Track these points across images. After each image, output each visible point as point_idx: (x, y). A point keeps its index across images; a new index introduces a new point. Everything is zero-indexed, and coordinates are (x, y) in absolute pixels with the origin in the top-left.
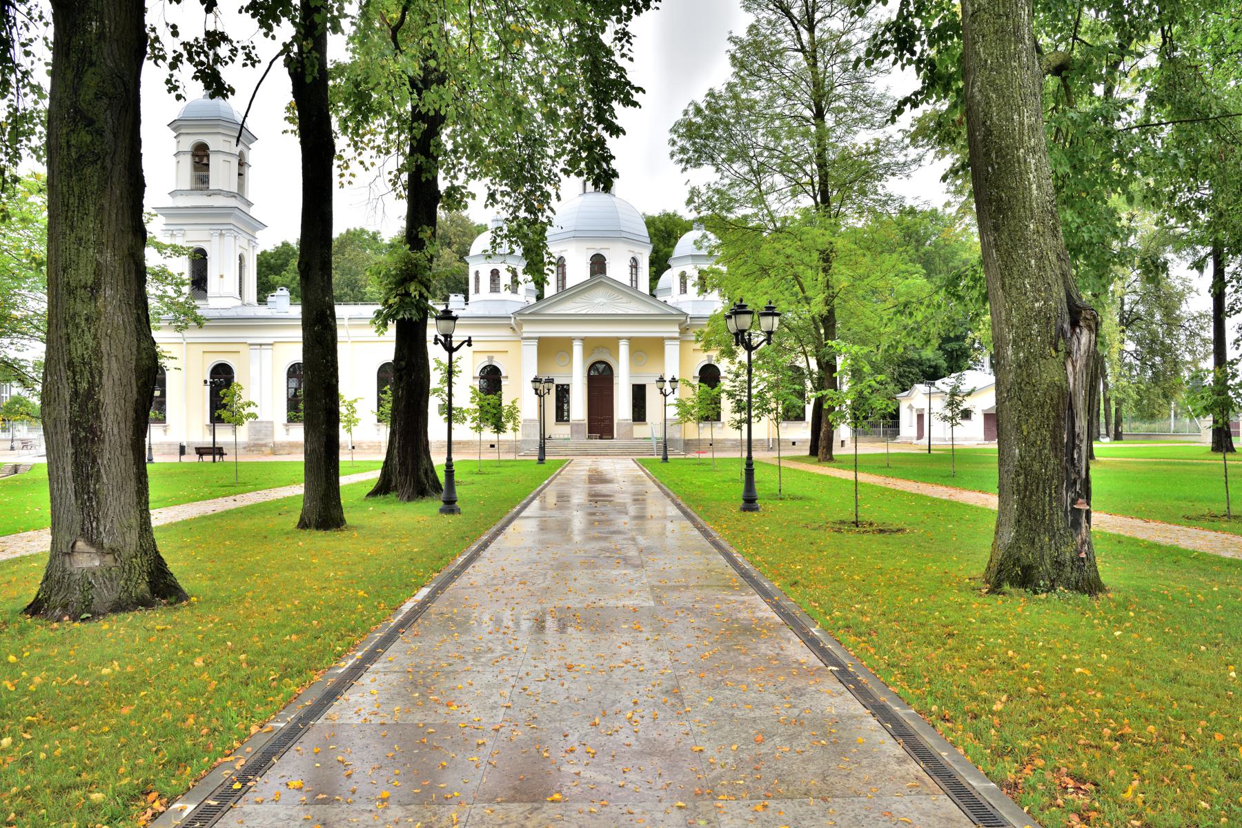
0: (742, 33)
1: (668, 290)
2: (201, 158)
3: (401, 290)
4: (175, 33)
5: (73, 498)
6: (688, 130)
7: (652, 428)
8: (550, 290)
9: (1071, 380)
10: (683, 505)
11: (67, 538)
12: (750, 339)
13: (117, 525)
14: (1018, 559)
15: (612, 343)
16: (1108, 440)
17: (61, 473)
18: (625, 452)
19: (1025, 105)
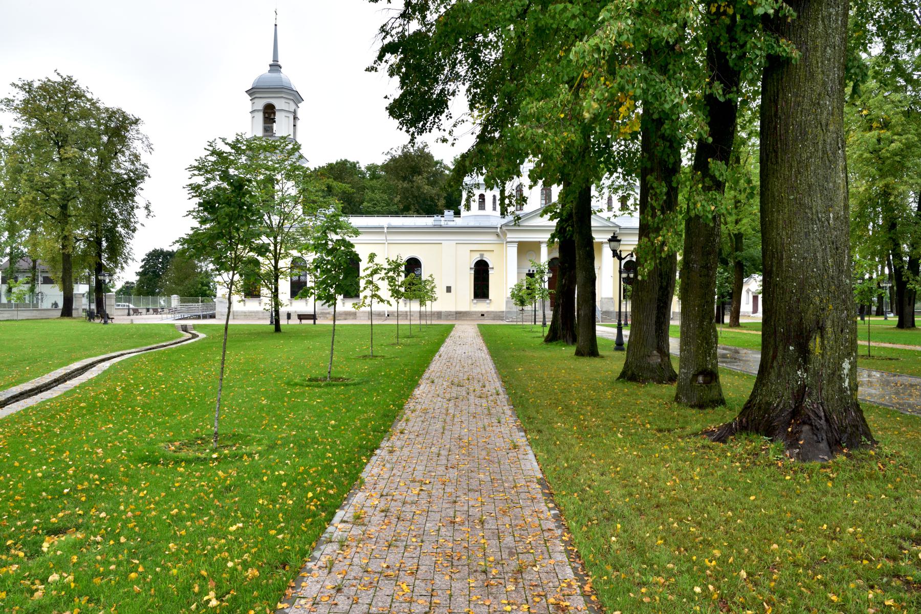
2: (270, 114)
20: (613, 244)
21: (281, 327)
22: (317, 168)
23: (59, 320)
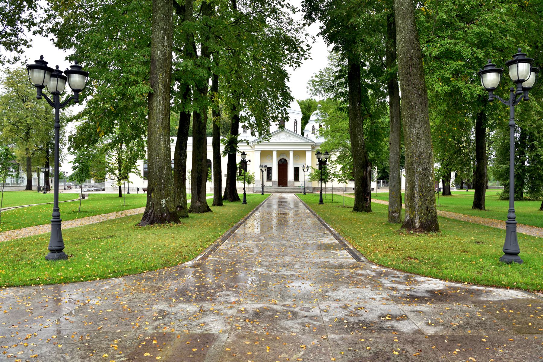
7: (300, 184)
15: (287, 152)
18: (291, 191)
20: (243, 156)
23: (26, 192)
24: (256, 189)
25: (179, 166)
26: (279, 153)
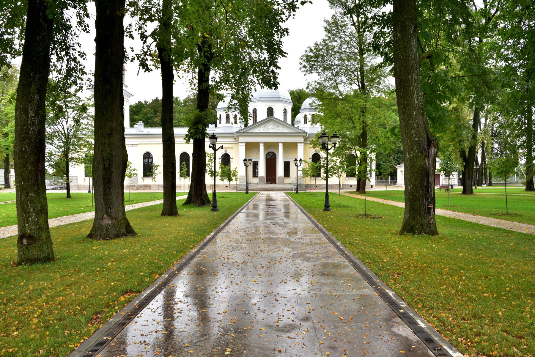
0: (330, 19)
1: (299, 122)
3: (196, 127)
4: (133, 51)
5: (103, 201)
6: (308, 59)
8: (251, 122)
9: (427, 164)
10: (302, 209)
11: (101, 214)
12: (327, 146)
13: (116, 210)
14: (410, 224)
15: (276, 145)
16: (485, 185)
17: (99, 193)
18: (281, 189)
19: (413, 72)
20: (212, 140)
21: (71, 195)
22: (143, 102)
24: (239, 187)
25: (23, 140)
26: (267, 145)
